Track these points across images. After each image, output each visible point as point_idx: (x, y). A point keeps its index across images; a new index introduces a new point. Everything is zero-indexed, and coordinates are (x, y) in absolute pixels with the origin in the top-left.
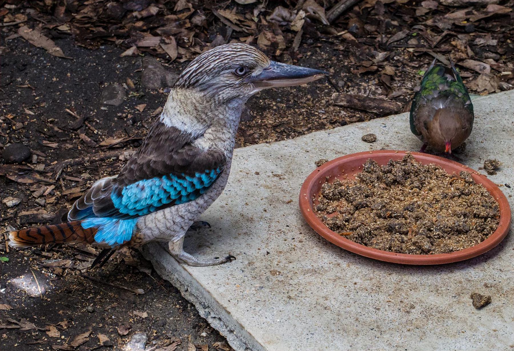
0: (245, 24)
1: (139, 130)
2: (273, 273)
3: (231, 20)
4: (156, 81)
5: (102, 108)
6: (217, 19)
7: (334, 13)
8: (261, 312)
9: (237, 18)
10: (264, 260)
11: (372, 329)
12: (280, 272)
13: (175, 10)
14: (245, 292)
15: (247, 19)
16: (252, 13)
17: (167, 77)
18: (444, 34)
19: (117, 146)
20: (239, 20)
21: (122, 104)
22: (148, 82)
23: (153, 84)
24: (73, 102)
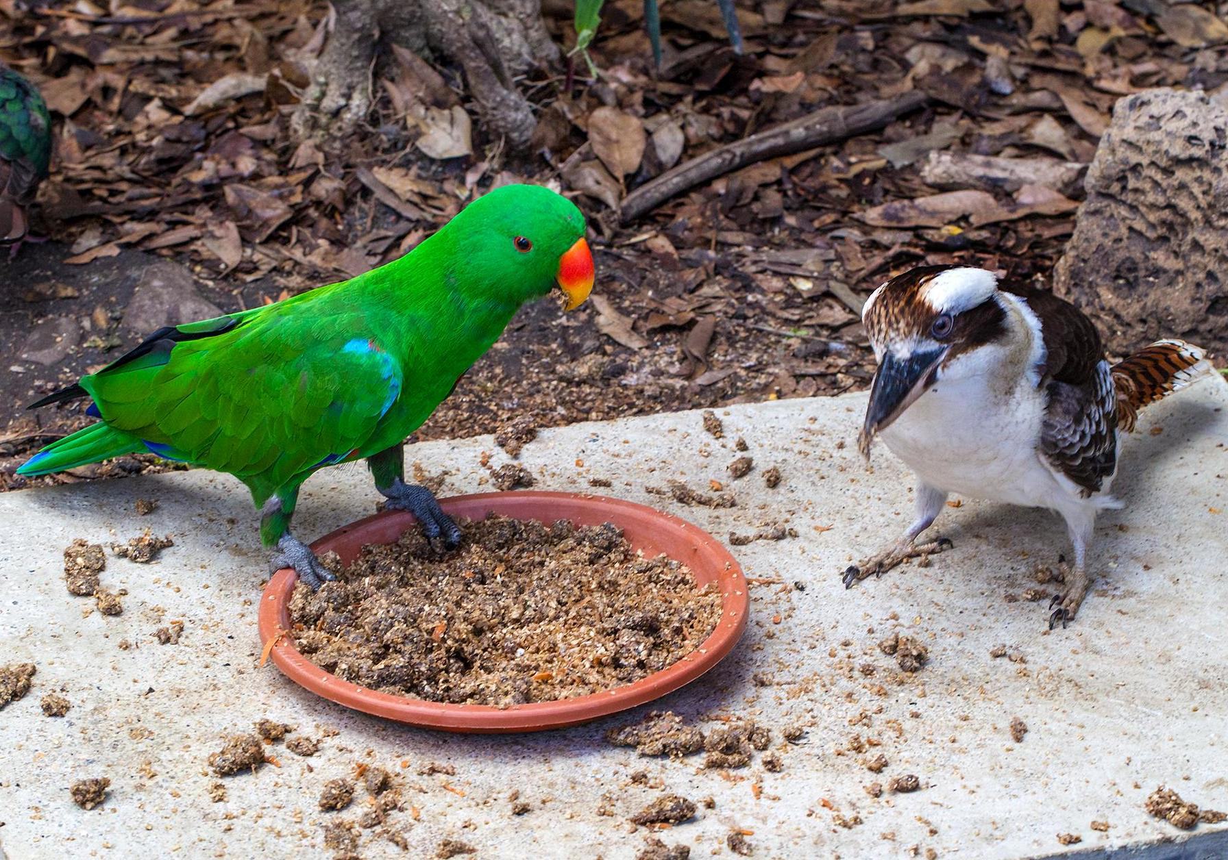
0: (436, 203)
1: (68, 418)
2: (136, 734)
3: (397, 191)
4: (155, 315)
5: (14, 368)
7: (648, 195)
9: (416, 189)
10: (132, 705)
12: (151, 733)
13: (290, 165)
14: (48, 769)
15: (445, 193)
16: (462, 182)
17: (182, 309)
18: (891, 253)
20: (420, 194)
21: (60, 362)
22: (136, 316)
23: (147, 321)
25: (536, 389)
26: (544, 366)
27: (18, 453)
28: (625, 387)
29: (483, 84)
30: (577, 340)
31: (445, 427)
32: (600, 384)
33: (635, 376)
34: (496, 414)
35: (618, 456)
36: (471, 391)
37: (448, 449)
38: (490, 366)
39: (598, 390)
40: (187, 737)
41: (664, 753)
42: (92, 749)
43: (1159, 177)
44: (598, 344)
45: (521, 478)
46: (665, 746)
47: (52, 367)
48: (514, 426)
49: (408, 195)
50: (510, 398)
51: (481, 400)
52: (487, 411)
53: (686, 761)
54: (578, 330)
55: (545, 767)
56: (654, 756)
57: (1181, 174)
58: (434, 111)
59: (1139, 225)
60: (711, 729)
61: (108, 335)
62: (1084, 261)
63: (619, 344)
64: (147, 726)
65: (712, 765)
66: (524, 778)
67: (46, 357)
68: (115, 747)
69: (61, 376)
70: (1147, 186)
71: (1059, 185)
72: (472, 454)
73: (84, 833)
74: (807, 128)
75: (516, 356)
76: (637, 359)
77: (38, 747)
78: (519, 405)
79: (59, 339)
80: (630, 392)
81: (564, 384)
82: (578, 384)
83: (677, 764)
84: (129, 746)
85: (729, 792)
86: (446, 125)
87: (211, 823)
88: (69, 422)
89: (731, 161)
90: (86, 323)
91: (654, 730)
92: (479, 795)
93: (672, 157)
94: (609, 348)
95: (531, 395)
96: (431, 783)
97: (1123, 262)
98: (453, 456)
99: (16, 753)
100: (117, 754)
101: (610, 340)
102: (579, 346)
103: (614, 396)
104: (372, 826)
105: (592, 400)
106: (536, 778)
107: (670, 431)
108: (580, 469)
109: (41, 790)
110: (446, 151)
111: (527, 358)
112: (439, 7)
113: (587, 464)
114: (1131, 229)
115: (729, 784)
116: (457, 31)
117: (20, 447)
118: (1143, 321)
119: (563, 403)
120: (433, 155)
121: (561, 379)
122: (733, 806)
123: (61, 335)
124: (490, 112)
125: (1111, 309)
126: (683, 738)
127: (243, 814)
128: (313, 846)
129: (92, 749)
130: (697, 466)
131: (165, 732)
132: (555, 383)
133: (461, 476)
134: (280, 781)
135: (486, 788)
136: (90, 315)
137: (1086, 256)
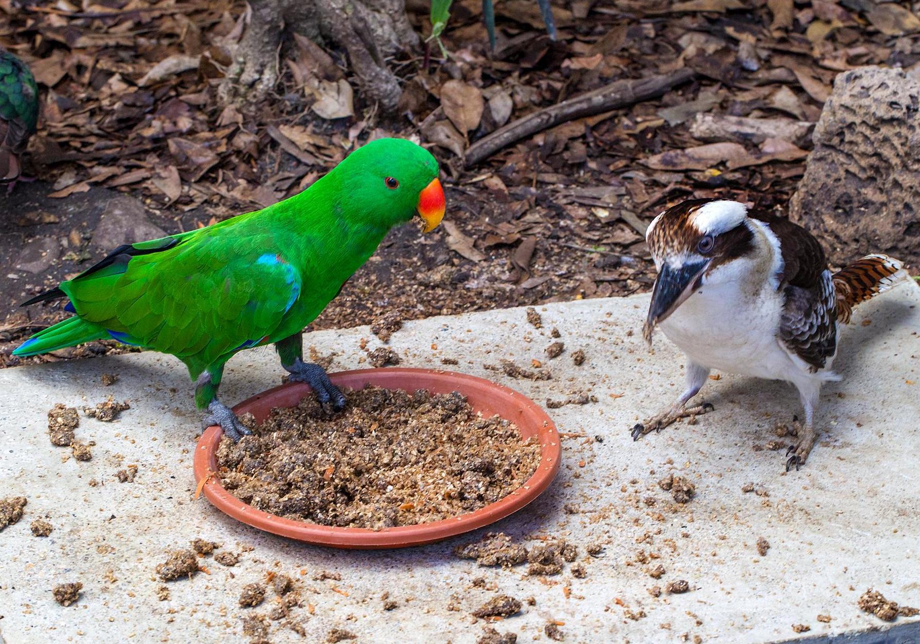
1: (51, 313)
2: (102, 550)
3: (298, 143)
4: (116, 236)
5: (11, 276)
6: (274, 144)
8: (42, 608)
9: (312, 142)
10: (99, 528)
12: (113, 549)
13: (217, 124)
14: (36, 576)
17: (136, 231)
18: (668, 189)
20: (314, 145)
21: (45, 271)
22: (102, 237)
23: (110, 241)
25: (401, 291)
26: (408, 274)
28: (468, 290)
29: (362, 63)
30: (432, 255)
31: (333, 320)
32: (449, 287)
33: (476, 282)
34: (371, 310)
35: (463, 341)
36: (353, 293)
37: (336, 336)
38: (367, 274)
39: (448, 292)
40: (140, 552)
41: (497, 564)
43: (868, 132)
44: (448, 257)
45: (390, 358)
46: (498, 559)
47: (39, 274)
48: (385, 319)
49: (306, 146)
50: (382, 298)
52: (365, 307)
53: (514, 570)
55: (408, 575)
56: (490, 566)
57: (885, 131)
58: (325, 83)
59: (853, 169)
60: (533, 546)
61: (81, 251)
62: (812, 195)
63: (464, 258)
64: (110, 543)
65: (534, 573)
67: (34, 267)
68: (86, 559)
69: (46, 282)
70: (860, 139)
71: (794, 138)
73: (63, 624)
74: (604, 96)
75: (387, 267)
77: (28, 560)
78: (389, 303)
79: (44, 254)
80: (472, 294)
81: (423, 288)
82: (433, 288)
83: (507, 572)
84: (97, 559)
85: (546, 593)
86: (334, 94)
87: (158, 616)
88: (52, 316)
89: (548, 120)
90: (65, 242)
92: (359, 595)
93: (504, 118)
94: (456, 261)
95: (398, 296)
96: (323, 586)
97: (842, 196)
98: (339, 341)
99: (12, 564)
100: (88, 565)
101: (457, 254)
103: (460, 297)
104: (278, 619)
105: (444, 300)
106: (402, 583)
107: (502, 323)
108: (435, 352)
110: (334, 113)
111: (395, 268)
112: (329, 5)
113: (439, 348)
114: (847, 171)
115: (546, 587)
116: (342, 23)
117: (15, 335)
118: (857, 241)
119: (422, 302)
120: (324, 116)
121: (420, 284)
123: (45, 251)
124: (367, 84)
125: (832, 231)
126: (512, 553)
127: (182, 610)
128: (235, 634)
129: (69, 561)
130: (522, 349)
132: (416, 287)
133: (345, 356)
134: (210, 585)
135: (364, 590)
136: (68, 236)
137: (814, 192)
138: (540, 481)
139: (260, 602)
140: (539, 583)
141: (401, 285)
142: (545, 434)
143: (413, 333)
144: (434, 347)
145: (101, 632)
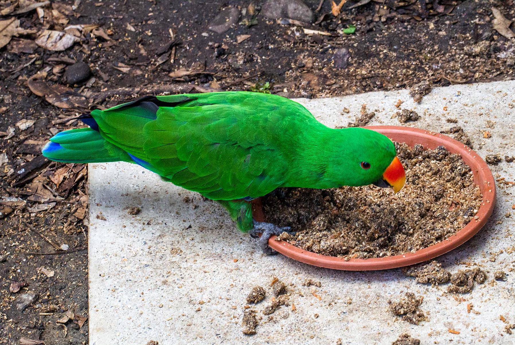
1: (220, 63)
4: (276, 10)
11: (312, 338)
12: (181, 251)
14: (126, 268)
17: (289, 7)
19: (182, 79)
22: (267, 10)
23: (272, 13)
24: (182, 24)
25: (453, 58)
26: (459, 46)
27: (190, 81)
28: (498, 59)
30: (481, 32)
31: (399, 78)
32: (485, 57)
33: (505, 53)
34: (427, 72)
35: (467, 105)
36: (418, 59)
38: (433, 44)
39: (484, 60)
40: (198, 255)
41: (428, 282)
42: (150, 258)
44: (490, 34)
45: (411, 117)
46: (429, 279)
48: (419, 87)
50: (438, 63)
51: (422, 63)
52: (423, 70)
53: (440, 287)
54: (483, 26)
55: (366, 286)
56: (424, 284)
60: (456, 271)
61: (252, 18)
63: (501, 35)
64: (181, 247)
65: (451, 291)
66: (354, 292)
67: (219, 29)
68: (161, 258)
69: (224, 40)
72: (394, 100)
75: (447, 40)
76: (508, 44)
77: (125, 256)
78: (441, 67)
79: (228, 20)
80: (500, 62)
81: (467, 56)
82: (474, 57)
83: (434, 289)
85: (455, 307)
87: (191, 306)
88: (219, 65)
90: (244, 12)
91: (425, 270)
92: (329, 299)
94: (495, 37)
95: (449, 62)
96: (307, 291)
98: (384, 101)
99: (114, 258)
100: (161, 262)
101: (497, 33)
102: (481, 35)
103: (491, 64)
104: (269, 314)
105: (479, 66)
106: (360, 292)
107: (498, 92)
108: (445, 112)
109: (118, 280)
111: (452, 41)
113: (449, 109)
115: (457, 303)
117: (192, 78)
119: (463, 67)
121: (466, 54)
122: (455, 316)
123: (229, 18)
126: (439, 275)
127: (209, 302)
128: (236, 324)
129: (150, 258)
130: (504, 113)
131: (188, 252)
132: (462, 55)
133: (384, 113)
134: (234, 284)
135: (333, 295)
136: (247, 7)
138: (469, 231)
139: (260, 301)
140: (453, 299)
141: (453, 53)
142: (486, 192)
143: (435, 97)
144: (445, 109)
145: (151, 315)
